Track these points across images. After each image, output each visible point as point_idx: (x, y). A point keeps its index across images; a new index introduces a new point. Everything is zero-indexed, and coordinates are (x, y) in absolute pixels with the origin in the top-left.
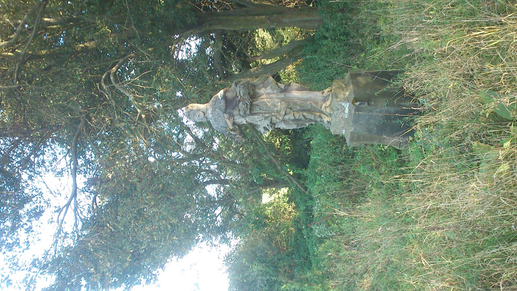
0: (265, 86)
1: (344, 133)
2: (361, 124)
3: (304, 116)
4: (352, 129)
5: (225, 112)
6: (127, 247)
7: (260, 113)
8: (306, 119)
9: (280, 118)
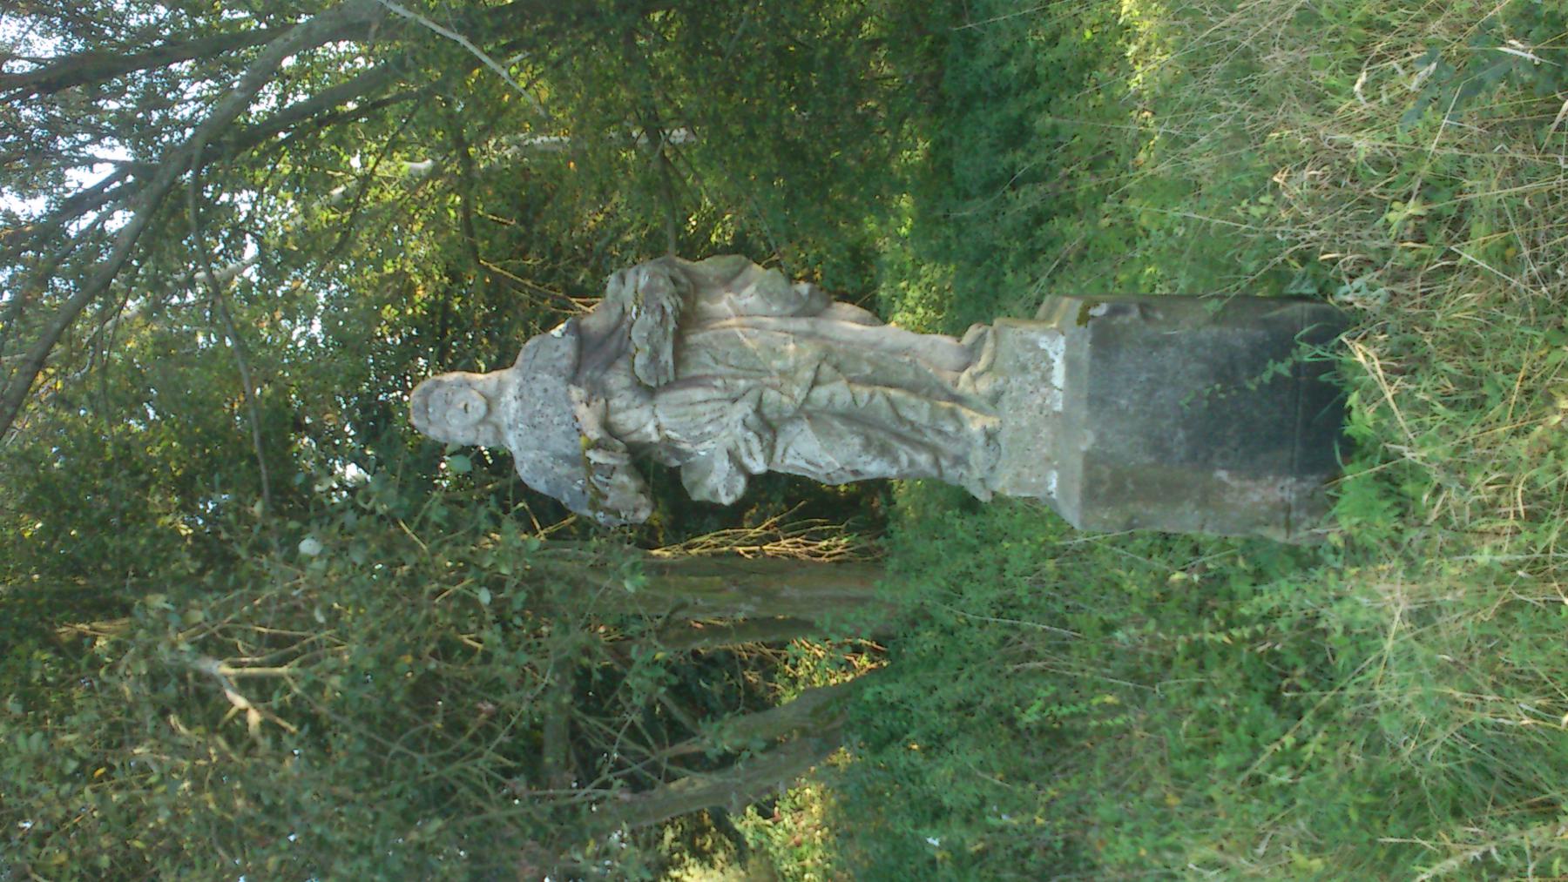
1: (1053, 485)
2: (1121, 413)
3: (888, 399)
4: (1087, 442)
5: (574, 380)
8: (901, 419)
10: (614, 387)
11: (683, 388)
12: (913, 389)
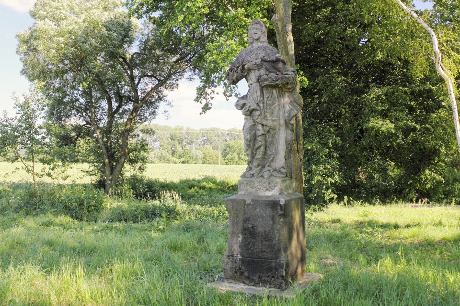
0: (292, 104)
1: (240, 193)
3: (260, 146)
6: (96, 31)
7: (263, 97)
8: (256, 150)
9: (259, 120)
10: (260, 71)
11: (260, 90)
12: (265, 153)
